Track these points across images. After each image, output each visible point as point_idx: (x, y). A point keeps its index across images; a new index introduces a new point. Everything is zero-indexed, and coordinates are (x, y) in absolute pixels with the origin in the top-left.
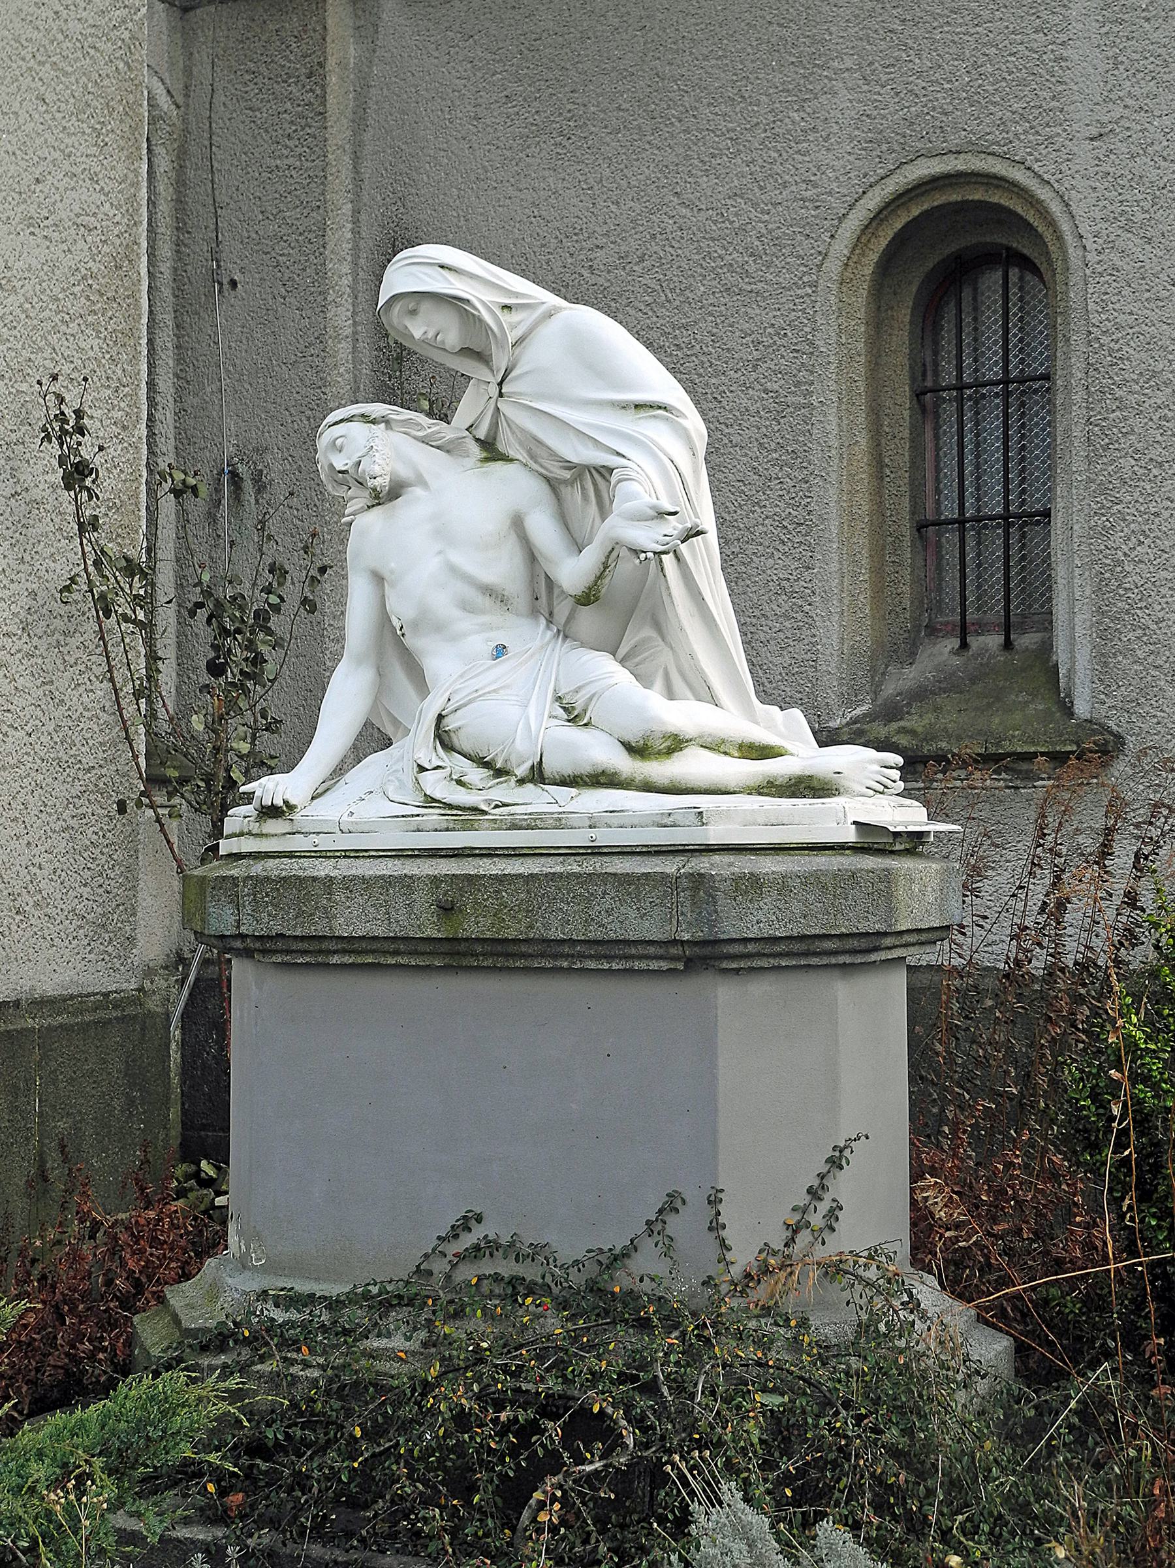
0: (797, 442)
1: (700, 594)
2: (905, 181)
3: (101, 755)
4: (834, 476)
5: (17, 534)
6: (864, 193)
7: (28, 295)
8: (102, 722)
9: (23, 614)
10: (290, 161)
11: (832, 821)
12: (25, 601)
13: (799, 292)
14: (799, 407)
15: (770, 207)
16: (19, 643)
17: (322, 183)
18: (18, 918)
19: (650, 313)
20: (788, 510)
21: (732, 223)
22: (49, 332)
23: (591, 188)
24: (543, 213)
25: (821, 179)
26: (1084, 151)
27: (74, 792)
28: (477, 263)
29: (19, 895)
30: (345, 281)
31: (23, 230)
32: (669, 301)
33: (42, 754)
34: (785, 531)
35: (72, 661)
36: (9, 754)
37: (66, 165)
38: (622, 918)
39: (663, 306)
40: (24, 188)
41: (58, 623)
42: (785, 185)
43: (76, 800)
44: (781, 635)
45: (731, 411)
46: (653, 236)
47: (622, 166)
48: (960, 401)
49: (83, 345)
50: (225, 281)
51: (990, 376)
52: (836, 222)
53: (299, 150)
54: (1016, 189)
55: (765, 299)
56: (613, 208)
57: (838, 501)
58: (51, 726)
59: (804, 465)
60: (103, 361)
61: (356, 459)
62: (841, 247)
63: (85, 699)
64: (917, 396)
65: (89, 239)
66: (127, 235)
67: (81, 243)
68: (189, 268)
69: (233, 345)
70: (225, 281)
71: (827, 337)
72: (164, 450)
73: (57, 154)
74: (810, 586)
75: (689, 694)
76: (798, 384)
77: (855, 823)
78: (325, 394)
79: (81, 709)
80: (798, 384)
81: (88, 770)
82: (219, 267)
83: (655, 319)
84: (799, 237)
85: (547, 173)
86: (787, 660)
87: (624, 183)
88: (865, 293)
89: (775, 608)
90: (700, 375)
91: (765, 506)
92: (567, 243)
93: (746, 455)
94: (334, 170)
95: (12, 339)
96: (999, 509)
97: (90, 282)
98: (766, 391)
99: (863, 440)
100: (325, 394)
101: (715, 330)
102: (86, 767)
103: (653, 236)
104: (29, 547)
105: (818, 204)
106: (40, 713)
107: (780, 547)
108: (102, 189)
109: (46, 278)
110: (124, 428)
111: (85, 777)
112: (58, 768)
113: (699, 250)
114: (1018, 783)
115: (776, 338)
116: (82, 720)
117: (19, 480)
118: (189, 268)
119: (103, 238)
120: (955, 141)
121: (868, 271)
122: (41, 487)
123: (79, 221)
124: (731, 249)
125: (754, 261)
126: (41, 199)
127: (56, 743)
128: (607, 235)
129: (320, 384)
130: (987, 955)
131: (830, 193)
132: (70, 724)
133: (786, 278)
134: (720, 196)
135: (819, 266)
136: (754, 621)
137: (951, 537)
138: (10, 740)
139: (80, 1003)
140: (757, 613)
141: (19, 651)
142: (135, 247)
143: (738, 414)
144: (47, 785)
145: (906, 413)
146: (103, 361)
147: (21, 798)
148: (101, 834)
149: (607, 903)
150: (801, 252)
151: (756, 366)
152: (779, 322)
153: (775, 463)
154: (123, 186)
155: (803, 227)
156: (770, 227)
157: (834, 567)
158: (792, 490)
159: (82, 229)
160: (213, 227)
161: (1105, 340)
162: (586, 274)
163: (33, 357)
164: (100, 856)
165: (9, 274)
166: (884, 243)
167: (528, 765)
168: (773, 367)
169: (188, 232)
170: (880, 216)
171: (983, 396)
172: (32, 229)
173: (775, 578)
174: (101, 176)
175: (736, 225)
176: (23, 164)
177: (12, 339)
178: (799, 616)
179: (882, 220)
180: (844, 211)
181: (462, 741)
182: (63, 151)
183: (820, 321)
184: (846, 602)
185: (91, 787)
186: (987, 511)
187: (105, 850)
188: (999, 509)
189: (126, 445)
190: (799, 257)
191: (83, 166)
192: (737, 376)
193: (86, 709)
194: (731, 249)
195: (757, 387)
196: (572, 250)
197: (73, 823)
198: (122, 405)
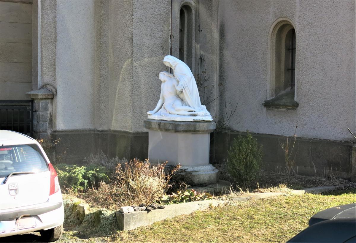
12: (151, 85)
26: (297, 18)
30: (215, 30)
35: (158, 91)
36: (148, 103)
37: (158, 31)
40: (151, 35)
57: (270, 67)
58: (155, 100)
62: (271, 30)
67: (160, 40)
71: (269, 44)
113: (255, 29)
120: (284, 16)
131: (270, 22)
135: (269, 33)
161: (299, 46)
166: (278, 29)
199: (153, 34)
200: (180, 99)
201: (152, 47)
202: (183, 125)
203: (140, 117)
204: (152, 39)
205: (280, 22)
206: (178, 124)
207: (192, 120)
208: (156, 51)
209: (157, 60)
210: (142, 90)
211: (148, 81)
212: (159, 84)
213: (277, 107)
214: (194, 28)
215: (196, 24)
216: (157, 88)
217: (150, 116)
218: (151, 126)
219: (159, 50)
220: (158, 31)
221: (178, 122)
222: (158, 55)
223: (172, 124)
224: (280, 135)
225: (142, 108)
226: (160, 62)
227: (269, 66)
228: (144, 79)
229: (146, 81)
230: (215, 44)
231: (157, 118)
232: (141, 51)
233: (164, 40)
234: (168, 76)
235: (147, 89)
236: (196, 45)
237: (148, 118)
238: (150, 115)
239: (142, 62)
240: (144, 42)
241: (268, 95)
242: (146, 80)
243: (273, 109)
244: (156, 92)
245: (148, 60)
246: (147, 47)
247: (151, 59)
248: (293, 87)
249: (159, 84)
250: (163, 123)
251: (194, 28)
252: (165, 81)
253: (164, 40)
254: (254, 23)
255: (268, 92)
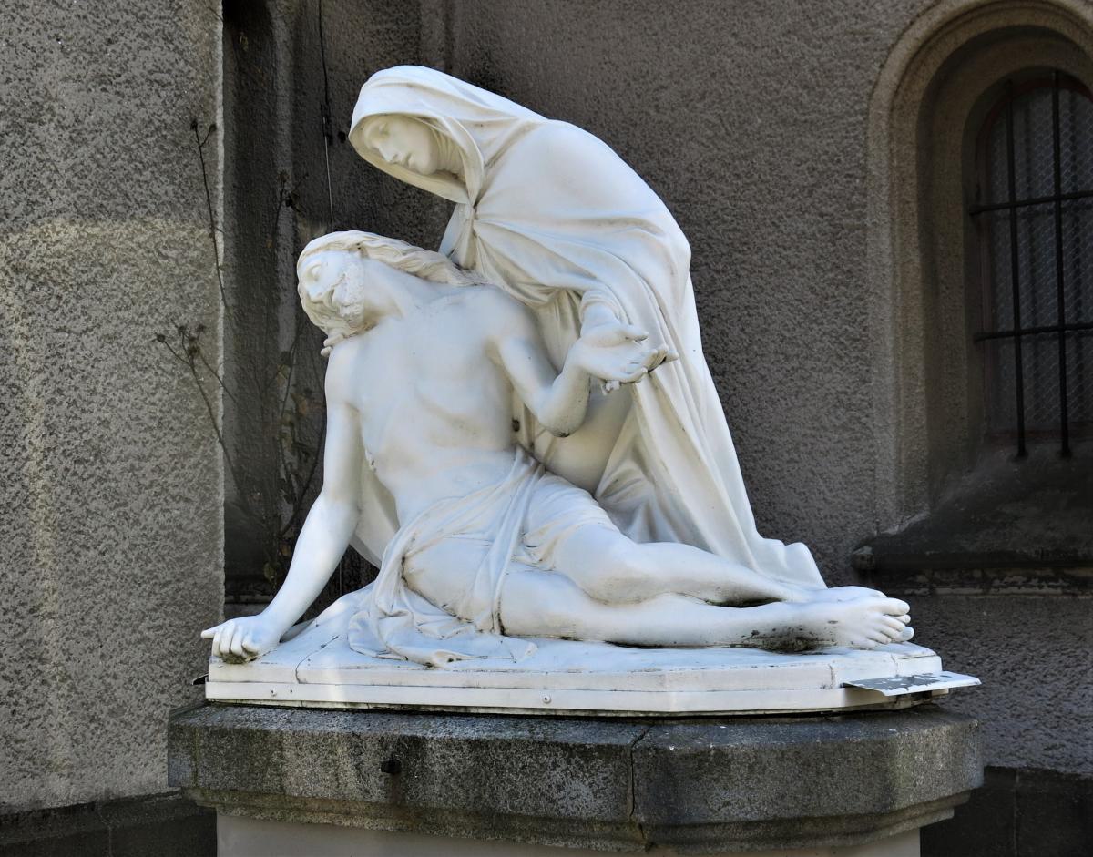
0: (852, 262)
1: (680, 424)
2: (951, 9)
3: (178, 570)
4: (888, 294)
5: (89, 367)
6: (912, 23)
7: (100, 146)
8: (179, 539)
9: (95, 441)
10: (389, 25)
11: (808, 686)
13: (851, 120)
14: (852, 229)
15: (822, 41)
16: (91, 470)
17: (417, 44)
18: (92, 726)
19: (712, 146)
20: (844, 327)
21: (785, 58)
22: (122, 180)
23: (656, 34)
24: (614, 59)
25: (870, 12)
27: (150, 605)
28: (450, 82)
29: (93, 704)
31: (94, 86)
32: (728, 134)
33: (116, 571)
34: (841, 347)
35: (147, 482)
36: (82, 573)
37: (139, 28)
38: (573, 794)
39: (723, 139)
40: (95, 48)
41: (131, 449)
42: (835, 20)
43: (153, 613)
44: (839, 445)
45: (788, 235)
46: (713, 75)
47: (684, 12)
48: (1013, 219)
49: (157, 190)
50: (335, 135)
51: (1044, 194)
52: (885, 53)
53: (396, 15)
54: (1061, 12)
55: (818, 128)
56: (676, 51)
57: (894, 316)
58: (126, 545)
59: (860, 283)
60: (179, 205)
61: (329, 289)
62: (890, 76)
63: (161, 518)
64: (972, 215)
65: (163, 94)
66: (202, 89)
67: (154, 98)
68: (305, 124)
69: (342, 191)
70: (335, 135)
71: (879, 160)
72: (286, 285)
73: (130, 18)
74: (867, 398)
75: (671, 533)
76: (852, 207)
77: (844, 686)
78: (420, 231)
79: (156, 528)
80: (852, 207)
81: (166, 584)
82: (328, 121)
83: (715, 151)
84: (850, 69)
85: (615, 22)
86: (846, 470)
87: (685, 28)
88: (916, 119)
89: (834, 420)
90: (759, 202)
91: (822, 324)
92: (635, 85)
93: (804, 275)
94: (427, 31)
95: (83, 187)
96: (1055, 322)
97: (164, 133)
98: (822, 215)
99: (916, 258)
100: (420, 231)
101: (772, 159)
102: (163, 581)
103: (713, 75)
104: (101, 379)
105: (868, 36)
106: (112, 532)
107: (837, 362)
108: (177, 47)
109: (118, 130)
110: (200, 266)
111: (163, 591)
112: (132, 584)
114: (1076, 590)
115: (830, 165)
116: (159, 538)
117: (90, 317)
118: (305, 124)
119: (177, 93)
121: (918, 97)
122: (114, 322)
123: (153, 77)
124: (786, 83)
125: (808, 94)
126: (113, 58)
127: (131, 560)
128: (671, 76)
129: (416, 222)
130: (1047, 759)
131: (879, 25)
132: (145, 541)
133: (838, 107)
134: (775, 34)
135: (870, 95)
136: (813, 432)
137: (1008, 349)
138: (82, 559)
139: (158, 802)
140: (816, 425)
141: (91, 476)
142: (211, 100)
143: (795, 237)
144: (122, 600)
145: (960, 232)
146: (179, 205)
147: (93, 613)
148: (179, 643)
149: (557, 777)
150: (853, 83)
151: (811, 193)
152: (833, 149)
153: (831, 282)
154: (198, 44)
155: (854, 58)
156: (823, 59)
157: (889, 380)
158: (848, 308)
159: (156, 85)
160: (324, 87)
162: (652, 112)
163: (105, 203)
164: (178, 664)
165: (80, 127)
166: (933, 70)
167: (488, 613)
168: (827, 191)
169: (304, 93)
170: (926, 45)
171: (1037, 214)
172: (104, 86)
173: (833, 391)
174: (175, 36)
175: (791, 60)
176: (95, 27)
177: (83, 187)
178: (857, 427)
179: (930, 48)
180: (891, 42)
181: (422, 583)
182: (136, 14)
183: (872, 145)
184: (903, 413)
185: (168, 600)
186: (1041, 324)
187: (183, 659)
188: (1055, 322)
189: (202, 281)
190: (850, 87)
191: (157, 27)
192: (794, 201)
193: (163, 527)
194: (786, 83)
195: (812, 210)
196: (639, 91)
197: (151, 634)
198: (198, 245)
199: (109, 42)
200: (562, 479)
201: (100, 140)
202: (755, 765)
203: (19, 686)
204: (101, 79)
205: (956, 19)
206: (700, 757)
207: (836, 700)
208: (128, 177)
209: (140, 245)
210: (31, 466)
211: (74, 395)
212: (154, 424)
213: (977, 574)
214: (284, 126)
215: (296, 106)
216: (139, 458)
217: (235, 672)
218: (271, 782)
219: (147, 175)
220: (139, 28)
221: (230, 713)
222: (142, 205)
223: (609, 752)
224: (1023, 763)
225: (31, 611)
226: (156, 263)
227: (887, 310)
228: (44, 383)
229: (58, 398)
230: (437, 209)
231: (335, 695)
232: (22, 160)
233: (180, 102)
234: (400, 268)
235: (68, 463)
236: (300, 226)
237: (213, 691)
238: (233, 659)
239: (29, 241)
240: (48, 96)
241: (889, 499)
242: (60, 391)
243: (941, 591)
244: (133, 485)
245: (72, 230)
246: (66, 134)
247: (96, 230)
248: (1027, 447)
249: (154, 424)
250: (448, 744)
251: (284, 126)
252: (367, 322)
253: (180, 102)
254: (742, 50)
255: (890, 478)
